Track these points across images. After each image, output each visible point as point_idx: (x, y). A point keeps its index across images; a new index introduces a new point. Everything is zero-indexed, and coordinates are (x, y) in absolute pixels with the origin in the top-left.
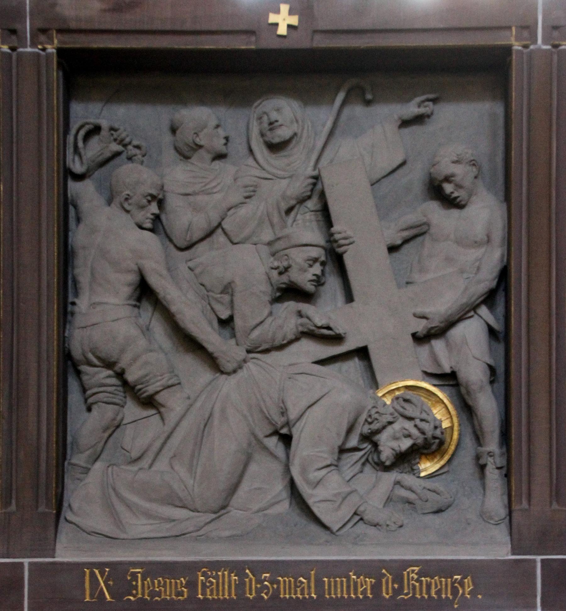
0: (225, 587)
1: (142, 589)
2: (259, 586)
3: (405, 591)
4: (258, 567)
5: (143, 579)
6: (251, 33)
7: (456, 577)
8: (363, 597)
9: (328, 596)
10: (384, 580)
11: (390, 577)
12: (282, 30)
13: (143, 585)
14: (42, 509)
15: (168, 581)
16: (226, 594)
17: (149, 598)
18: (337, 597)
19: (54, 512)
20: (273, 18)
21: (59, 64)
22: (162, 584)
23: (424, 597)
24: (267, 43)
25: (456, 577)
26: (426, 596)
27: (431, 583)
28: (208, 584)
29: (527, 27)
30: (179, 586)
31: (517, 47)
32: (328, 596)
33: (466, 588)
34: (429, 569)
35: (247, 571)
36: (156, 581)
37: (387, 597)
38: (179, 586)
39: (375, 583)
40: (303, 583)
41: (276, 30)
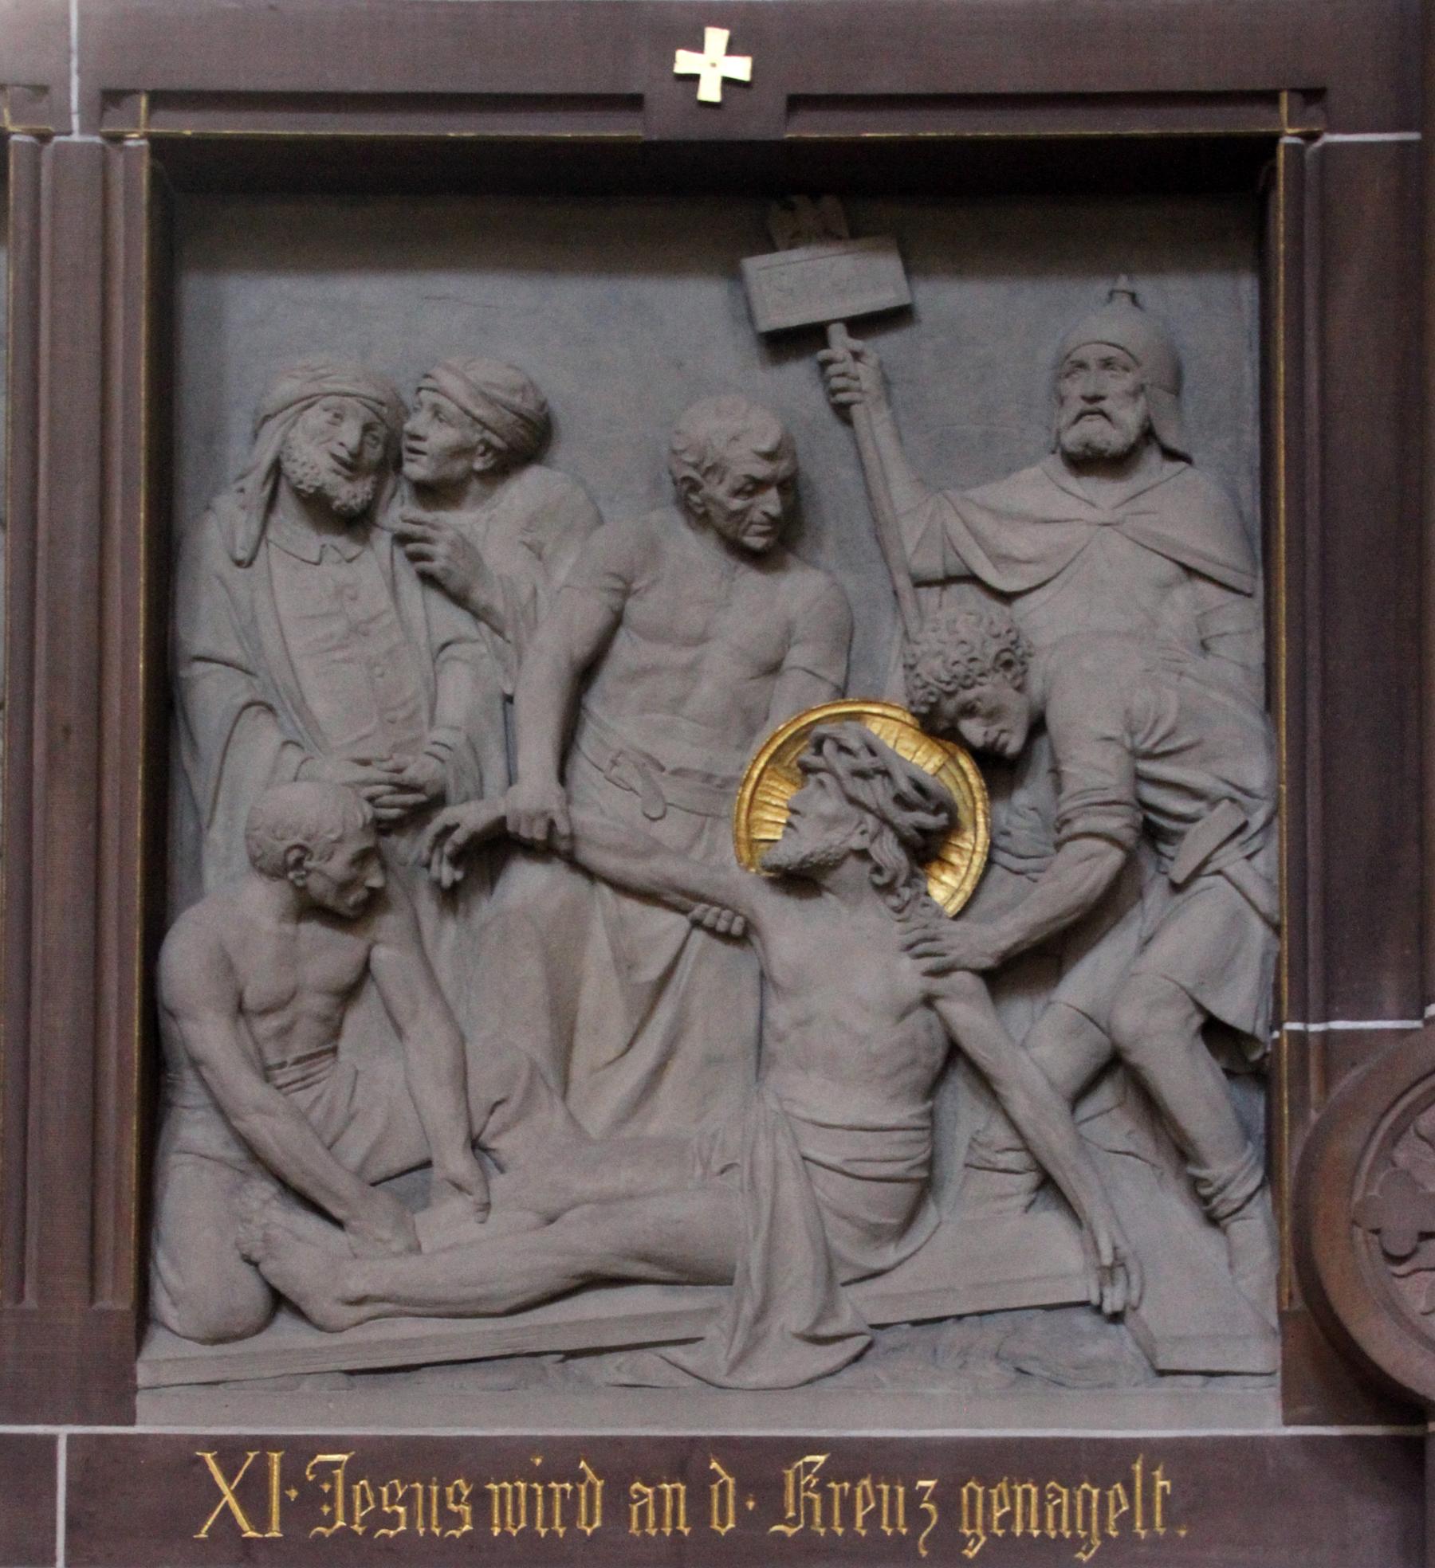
2: (293, 1494)
3: (791, 1514)
5: (350, 1480)
6: (634, 102)
7: (922, 1483)
8: (1072, 1536)
9: (889, 1531)
11: (599, 1483)
13: (348, 1493)
14: (105, 1303)
16: (1050, 1523)
20: (685, 62)
21: (155, 176)
23: (556, 1533)
25: (922, 1483)
26: (1068, 1534)
27: (576, 1492)
28: (1050, 1496)
29: (42, 90)
31: (1289, 138)
33: (995, 1507)
34: (379, 1460)
35: (714, 1465)
36: (385, 1490)
37: (589, 1531)
40: (643, 1496)
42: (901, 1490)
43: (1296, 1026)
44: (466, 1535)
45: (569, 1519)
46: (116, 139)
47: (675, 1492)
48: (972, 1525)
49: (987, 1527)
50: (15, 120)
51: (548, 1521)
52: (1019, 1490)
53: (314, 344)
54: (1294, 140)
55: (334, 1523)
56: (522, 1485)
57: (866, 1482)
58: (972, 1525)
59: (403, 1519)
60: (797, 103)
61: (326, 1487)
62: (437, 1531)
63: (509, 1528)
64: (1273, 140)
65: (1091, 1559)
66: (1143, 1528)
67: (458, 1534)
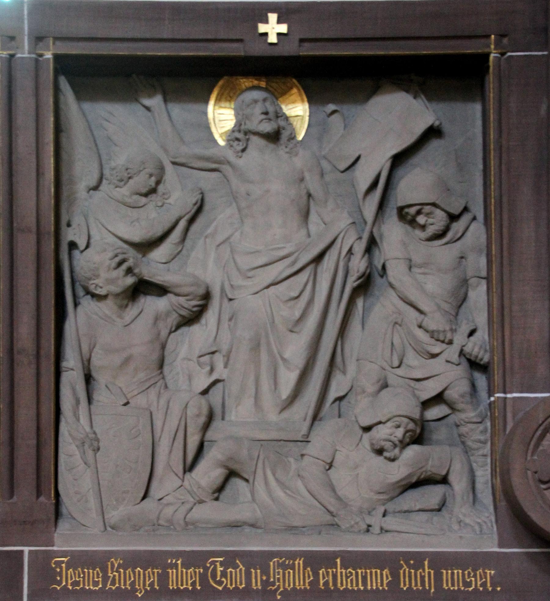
0: (182, 578)
1: (68, 578)
4: (416, 560)
5: (67, 569)
6: (240, 41)
8: (364, 589)
10: (402, 572)
11: (244, 569)
12: (273, 39)
13: (67, 574)
15: (368, 571)
16: (175, 585)
17: (70, 588)
18: (173, 588)
19: (54, 501)
20: (262, 28)
22: (472, 576)
24: (255, 49)
29: (12, 38)
30: (466, 577)
32: (123, 587)
35: (238, 561)
38: (466, 577)
39: (494, 574)
41: (266, 40)
42: (259, 571)
43: (502, 395)
44: (100, 588)
45: (365, 583)
46: (41, 55)
47: (458, 573)
48: (139, 586)
49: (144, 585)
50: (495, 49)
51: (416, 585)
52: (287, 572)
53: (123, 131)
54: (496, 55)
55: (62, 583)
56: (368, 571)
57: (80, 569)
58: (139, 586)
59: (474, 583)
60: (302, 41)
61: (58, 570)
62: (462, 588)
63: (179, 586)
64: (487, 55)
65: (142, 595)
66: (491, 586)
67: (78, 588)
